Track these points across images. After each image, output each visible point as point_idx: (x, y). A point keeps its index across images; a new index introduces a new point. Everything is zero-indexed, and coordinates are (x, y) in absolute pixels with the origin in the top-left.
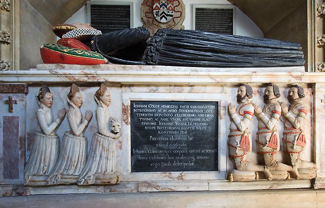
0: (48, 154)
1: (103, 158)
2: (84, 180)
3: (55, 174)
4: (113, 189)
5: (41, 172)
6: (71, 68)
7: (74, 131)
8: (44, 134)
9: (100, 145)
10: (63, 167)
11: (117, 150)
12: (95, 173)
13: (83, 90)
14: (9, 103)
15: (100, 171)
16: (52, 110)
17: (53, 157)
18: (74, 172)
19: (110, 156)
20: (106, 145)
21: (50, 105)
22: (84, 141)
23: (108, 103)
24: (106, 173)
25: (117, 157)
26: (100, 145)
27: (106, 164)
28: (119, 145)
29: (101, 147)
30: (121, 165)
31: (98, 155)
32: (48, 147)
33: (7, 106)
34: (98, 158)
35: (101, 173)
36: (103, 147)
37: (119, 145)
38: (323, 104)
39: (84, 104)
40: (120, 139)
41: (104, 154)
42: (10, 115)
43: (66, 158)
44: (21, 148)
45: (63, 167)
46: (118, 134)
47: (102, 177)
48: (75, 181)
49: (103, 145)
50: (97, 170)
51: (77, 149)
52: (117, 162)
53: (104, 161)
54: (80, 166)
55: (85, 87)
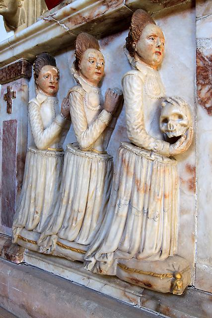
0: (40, 189)
1: (134, 210)
2: (93, 260)
3: (48, 232)
4: (163, 306)
5: (30, 223)
6: (19, 13)
7: (37, 145)
8: (36, 148)
9: (127, 173)
10: (60, 220)
11: (182, 191)
12: (118, 249)
13: (106, 44)
14: (8, 97)
15: (126, 245)
16: (57, 100)
17: (49, 197)
18: (80, 235)
19: (156, 207)
20: (143, 173)
21: (51, 90)
22: (101, 165)
23: (155, 57)
24: (141, 256)
25: (183, 211)
26: (127, 173)
27: (144, 228)
28: (187, 177)
29: (131, 180)
30: (193, 237)
31: (124, 200)
32: (42, 171)
33: (4, 105)
34: (123, 211)
35: (129, 253)
36: (136, 182)
37: (187, 177)
38: (43, 317)
39: (108, 77)
40: (191, 160)
41: (139, 201)
42: (9, 118)
43: (65, 200)
44: (18, 175)
45: (60, 220)
46: (178, 143)
47: (131, 264)
48: (79, 257)
49: (135, 174)
50: (122, 243)
51: (83, 181)
52: (182, 227)
53: (136, 222)
54: (91, 223)
55: (110, 38)
